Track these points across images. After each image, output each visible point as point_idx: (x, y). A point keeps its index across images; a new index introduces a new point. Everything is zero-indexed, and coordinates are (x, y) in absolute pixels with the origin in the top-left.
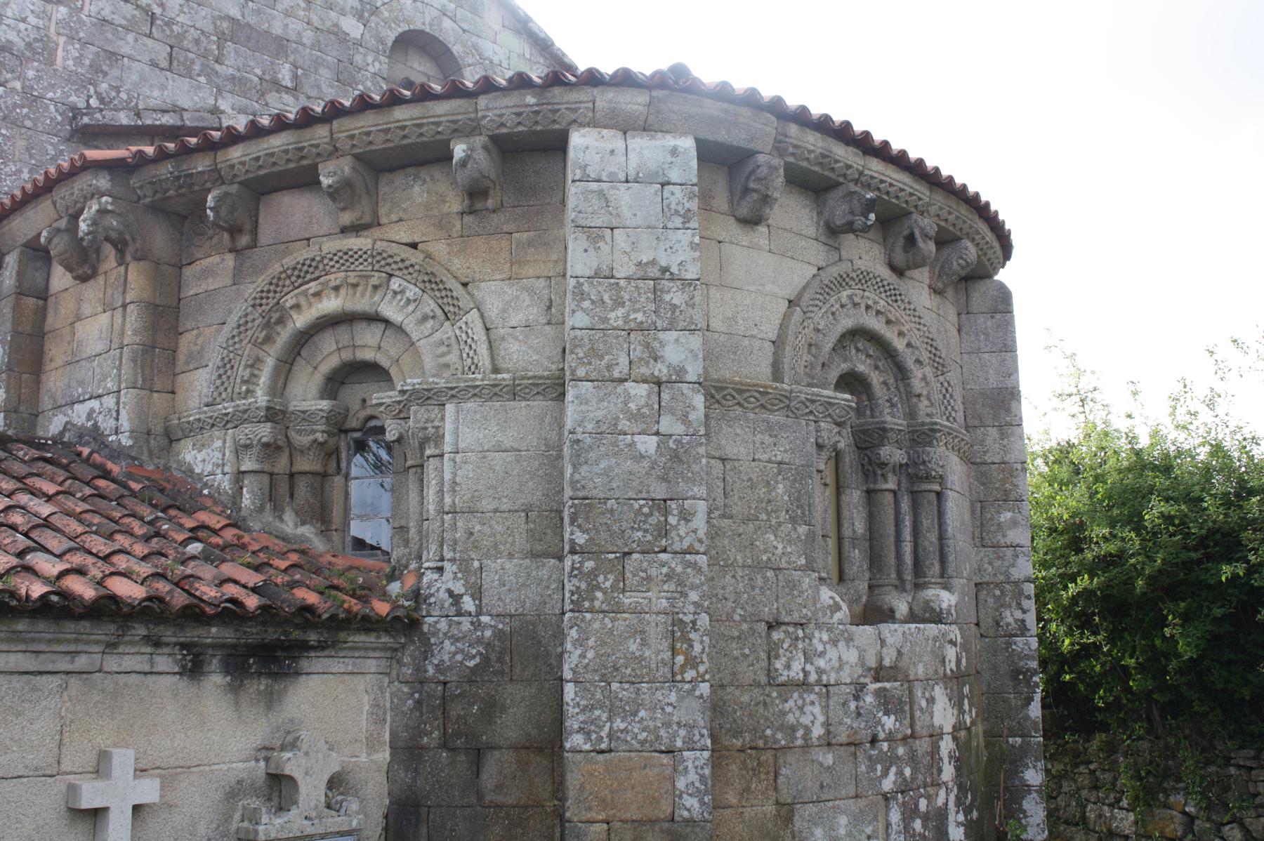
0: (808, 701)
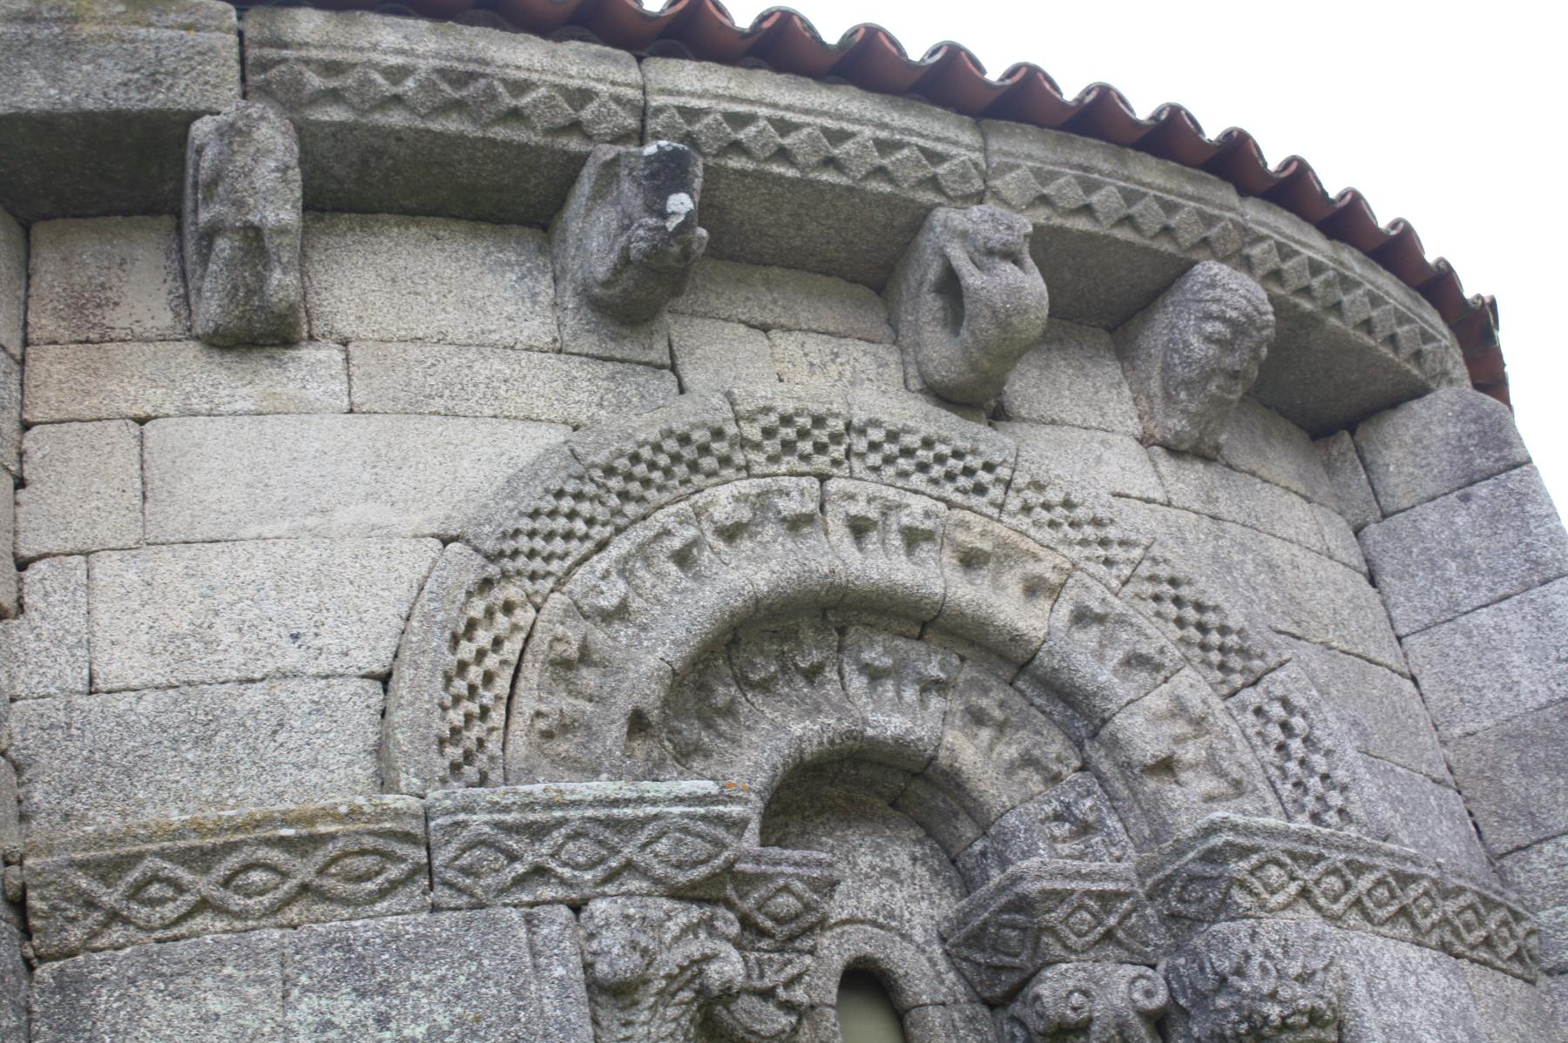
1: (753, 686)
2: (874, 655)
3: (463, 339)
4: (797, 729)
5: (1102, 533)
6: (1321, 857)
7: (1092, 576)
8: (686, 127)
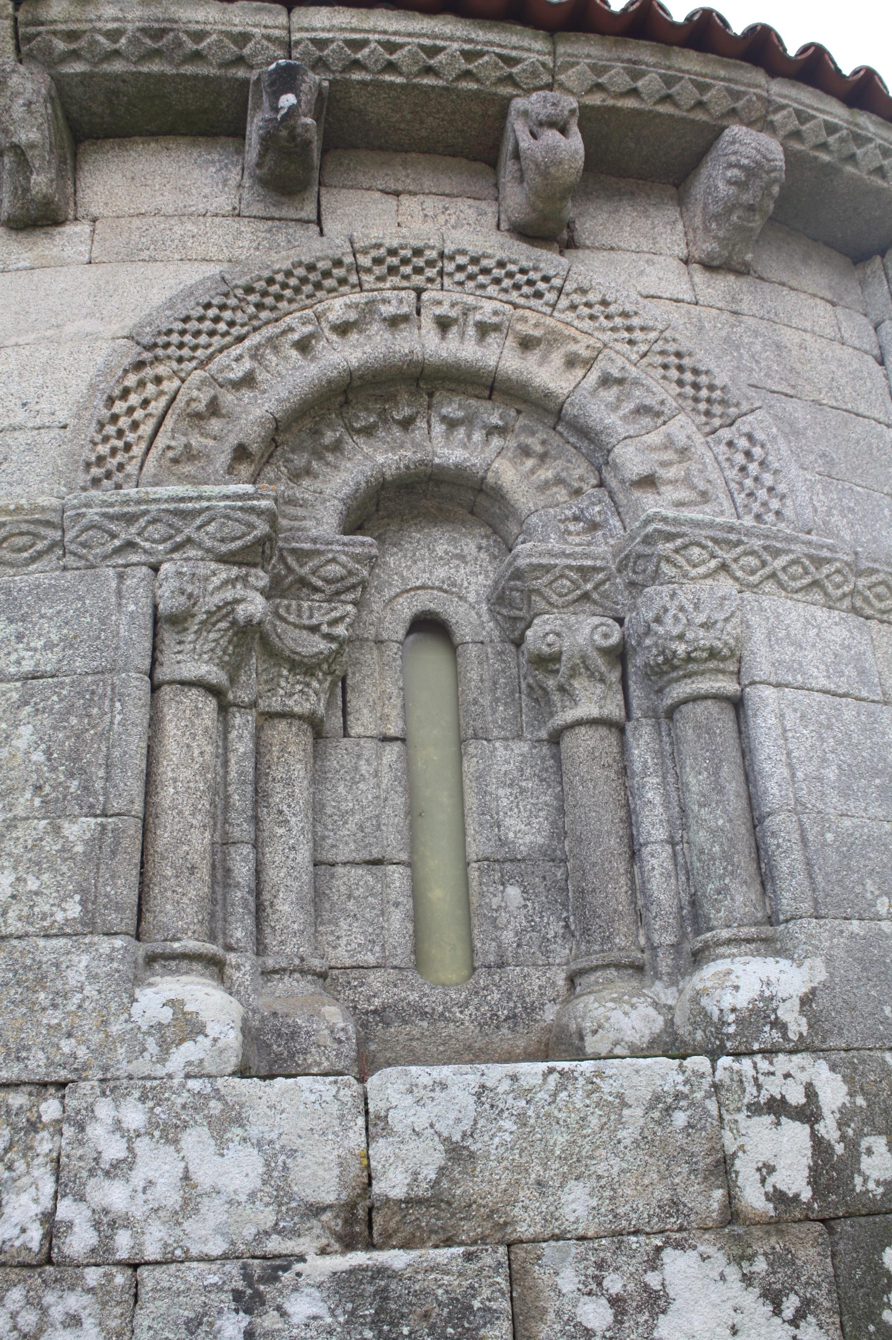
0: (56, 1314)
1: (359, 432)
2: (452, 410)
3: (171, 211)
4: (380, 459)
5: (628, 322)
6: (739, 543)
7: (617, 352)
8: (318, 53)
